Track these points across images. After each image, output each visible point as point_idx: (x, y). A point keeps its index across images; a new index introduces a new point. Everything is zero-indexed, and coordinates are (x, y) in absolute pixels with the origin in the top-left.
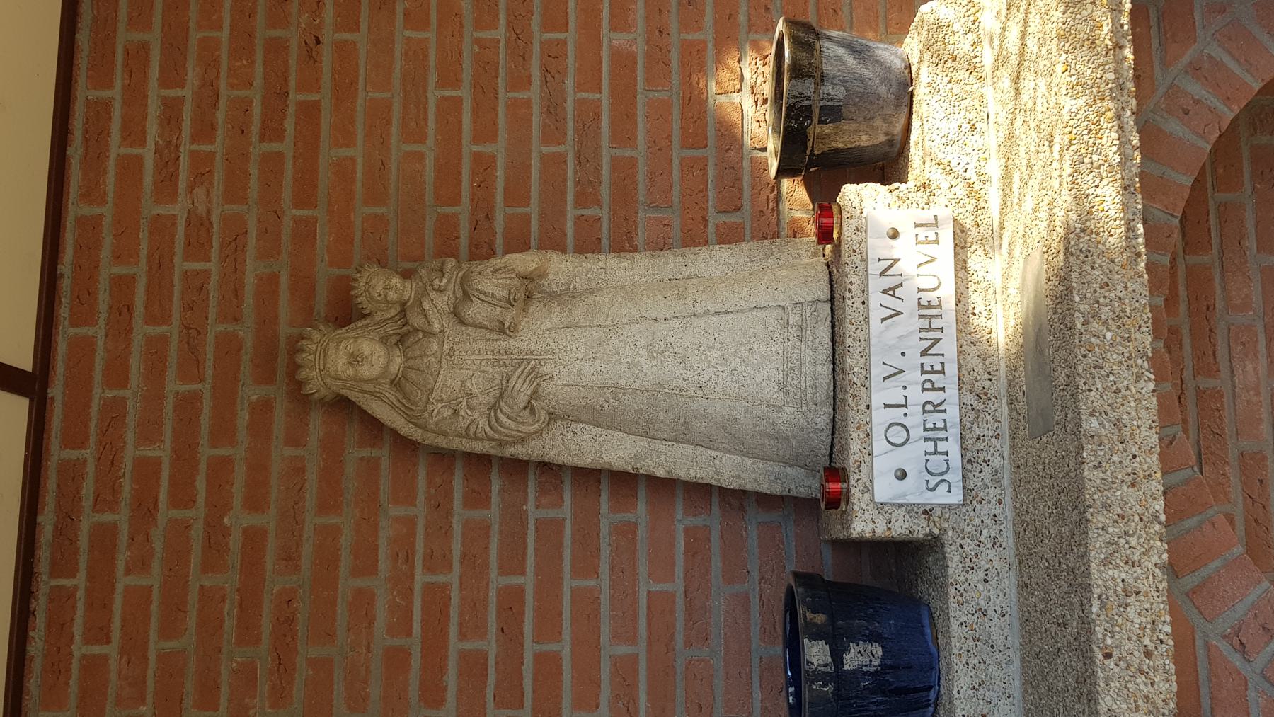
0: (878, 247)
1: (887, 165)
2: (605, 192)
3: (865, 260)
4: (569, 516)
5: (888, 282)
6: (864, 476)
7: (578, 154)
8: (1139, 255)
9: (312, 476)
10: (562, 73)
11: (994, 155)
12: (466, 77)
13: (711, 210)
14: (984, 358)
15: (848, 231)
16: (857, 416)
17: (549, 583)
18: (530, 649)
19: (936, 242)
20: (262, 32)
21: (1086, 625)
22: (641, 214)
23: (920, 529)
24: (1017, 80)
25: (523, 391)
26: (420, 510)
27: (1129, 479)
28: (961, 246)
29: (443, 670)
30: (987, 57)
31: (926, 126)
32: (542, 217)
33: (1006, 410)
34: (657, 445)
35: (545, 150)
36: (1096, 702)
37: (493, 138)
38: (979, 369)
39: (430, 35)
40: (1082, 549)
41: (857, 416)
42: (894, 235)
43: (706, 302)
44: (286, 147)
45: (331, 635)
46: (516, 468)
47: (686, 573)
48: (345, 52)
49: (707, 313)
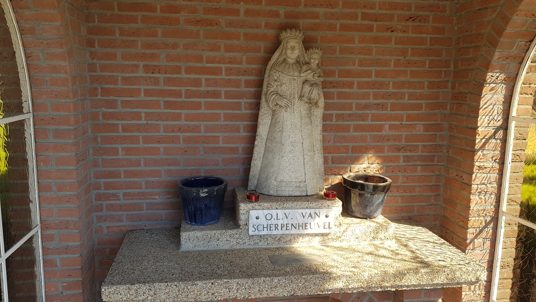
0: (323, 212)
1: (347, 212)
2: (340, 123)
3: (319, 208)
4: (242, 112)
5: (313, 215)
6: (257, 207)
7: (352, 115)
8: (323, 292)
9: (255, 31)
10: (378, 109)
11: (349, 244)
12: (378, 79)
13: (333, 155)
14: (290, 241)
15: (329, 203)
16: (274, 205)
17: (223, 106)
18: (203, 100)
19: (324, 228)
20: (396, 13)
21: (220, 277)
22: (332, 134)
23: (242, 223)
24: (371, 253)
25: (282, 103)
26: (244, 66)
27: (261, 290)
28: (322, 235)
29: (196, 73)
30: (377, 242)
31: (358, 225)
32: (333, 103)
33: (275, 246)
34: (264, 142)
35: (354, 104)
36: (199, 280)
37: (359, 88)
38: (287, 239)
39: (392, 68)
40: (241, 276)
41: (274, 205)
42: (327, 216)
43: (307, 158)
44: (359, 21)
45: (206, 38)
46: (258, 96)
47: (225, 147)
48: (388, 40)
49: (304, 159)
